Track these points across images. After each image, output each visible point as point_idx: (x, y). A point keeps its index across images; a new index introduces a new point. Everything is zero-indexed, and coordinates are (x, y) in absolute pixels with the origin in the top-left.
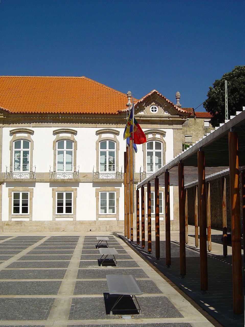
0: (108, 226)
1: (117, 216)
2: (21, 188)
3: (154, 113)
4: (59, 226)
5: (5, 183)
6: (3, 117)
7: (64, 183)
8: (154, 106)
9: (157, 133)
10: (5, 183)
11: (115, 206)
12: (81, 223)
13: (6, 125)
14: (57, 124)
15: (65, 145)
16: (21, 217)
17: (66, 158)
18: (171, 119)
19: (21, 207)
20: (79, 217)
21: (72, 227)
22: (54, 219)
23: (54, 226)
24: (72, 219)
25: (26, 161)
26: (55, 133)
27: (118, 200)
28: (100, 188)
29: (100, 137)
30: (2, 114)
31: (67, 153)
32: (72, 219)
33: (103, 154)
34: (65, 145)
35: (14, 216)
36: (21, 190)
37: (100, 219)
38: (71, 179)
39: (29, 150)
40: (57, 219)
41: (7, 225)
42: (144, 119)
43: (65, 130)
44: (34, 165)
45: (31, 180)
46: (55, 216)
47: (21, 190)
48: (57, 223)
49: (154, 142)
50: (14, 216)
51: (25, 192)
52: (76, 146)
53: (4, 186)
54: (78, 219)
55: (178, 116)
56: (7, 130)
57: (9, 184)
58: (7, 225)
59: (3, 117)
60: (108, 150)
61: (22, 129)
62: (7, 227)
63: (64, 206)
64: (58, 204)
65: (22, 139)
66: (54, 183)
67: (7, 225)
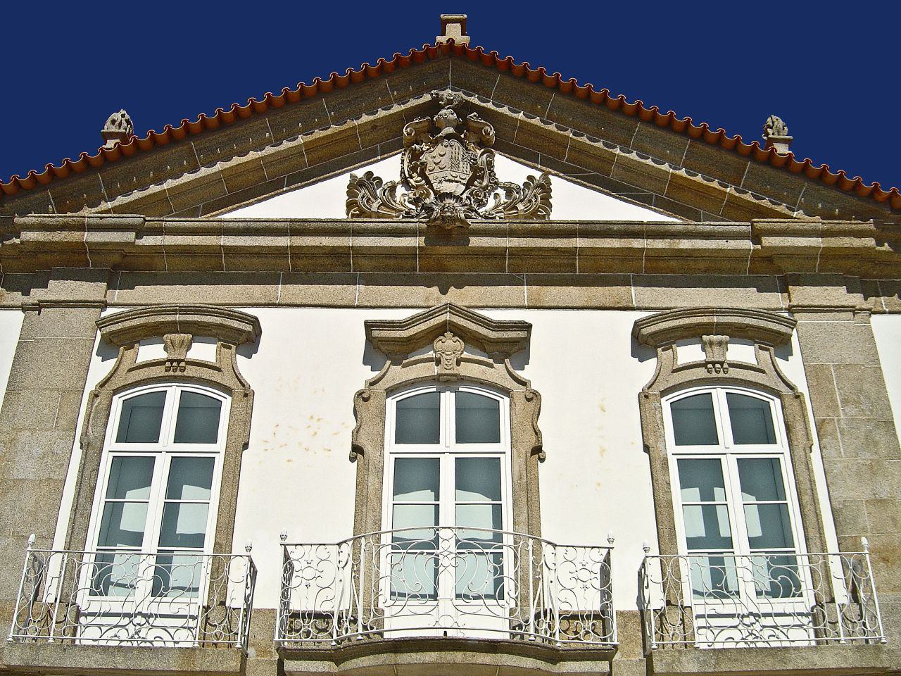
6: (870, 242)
9: (201, 332)
17: (459, 510)
30: (870, 225)
31: (467, 473)
39: (218, 449)
44: (238, 548)
49: (719, 396)
52: (243, 421)
60: (728, 450)
62: (335, 432)
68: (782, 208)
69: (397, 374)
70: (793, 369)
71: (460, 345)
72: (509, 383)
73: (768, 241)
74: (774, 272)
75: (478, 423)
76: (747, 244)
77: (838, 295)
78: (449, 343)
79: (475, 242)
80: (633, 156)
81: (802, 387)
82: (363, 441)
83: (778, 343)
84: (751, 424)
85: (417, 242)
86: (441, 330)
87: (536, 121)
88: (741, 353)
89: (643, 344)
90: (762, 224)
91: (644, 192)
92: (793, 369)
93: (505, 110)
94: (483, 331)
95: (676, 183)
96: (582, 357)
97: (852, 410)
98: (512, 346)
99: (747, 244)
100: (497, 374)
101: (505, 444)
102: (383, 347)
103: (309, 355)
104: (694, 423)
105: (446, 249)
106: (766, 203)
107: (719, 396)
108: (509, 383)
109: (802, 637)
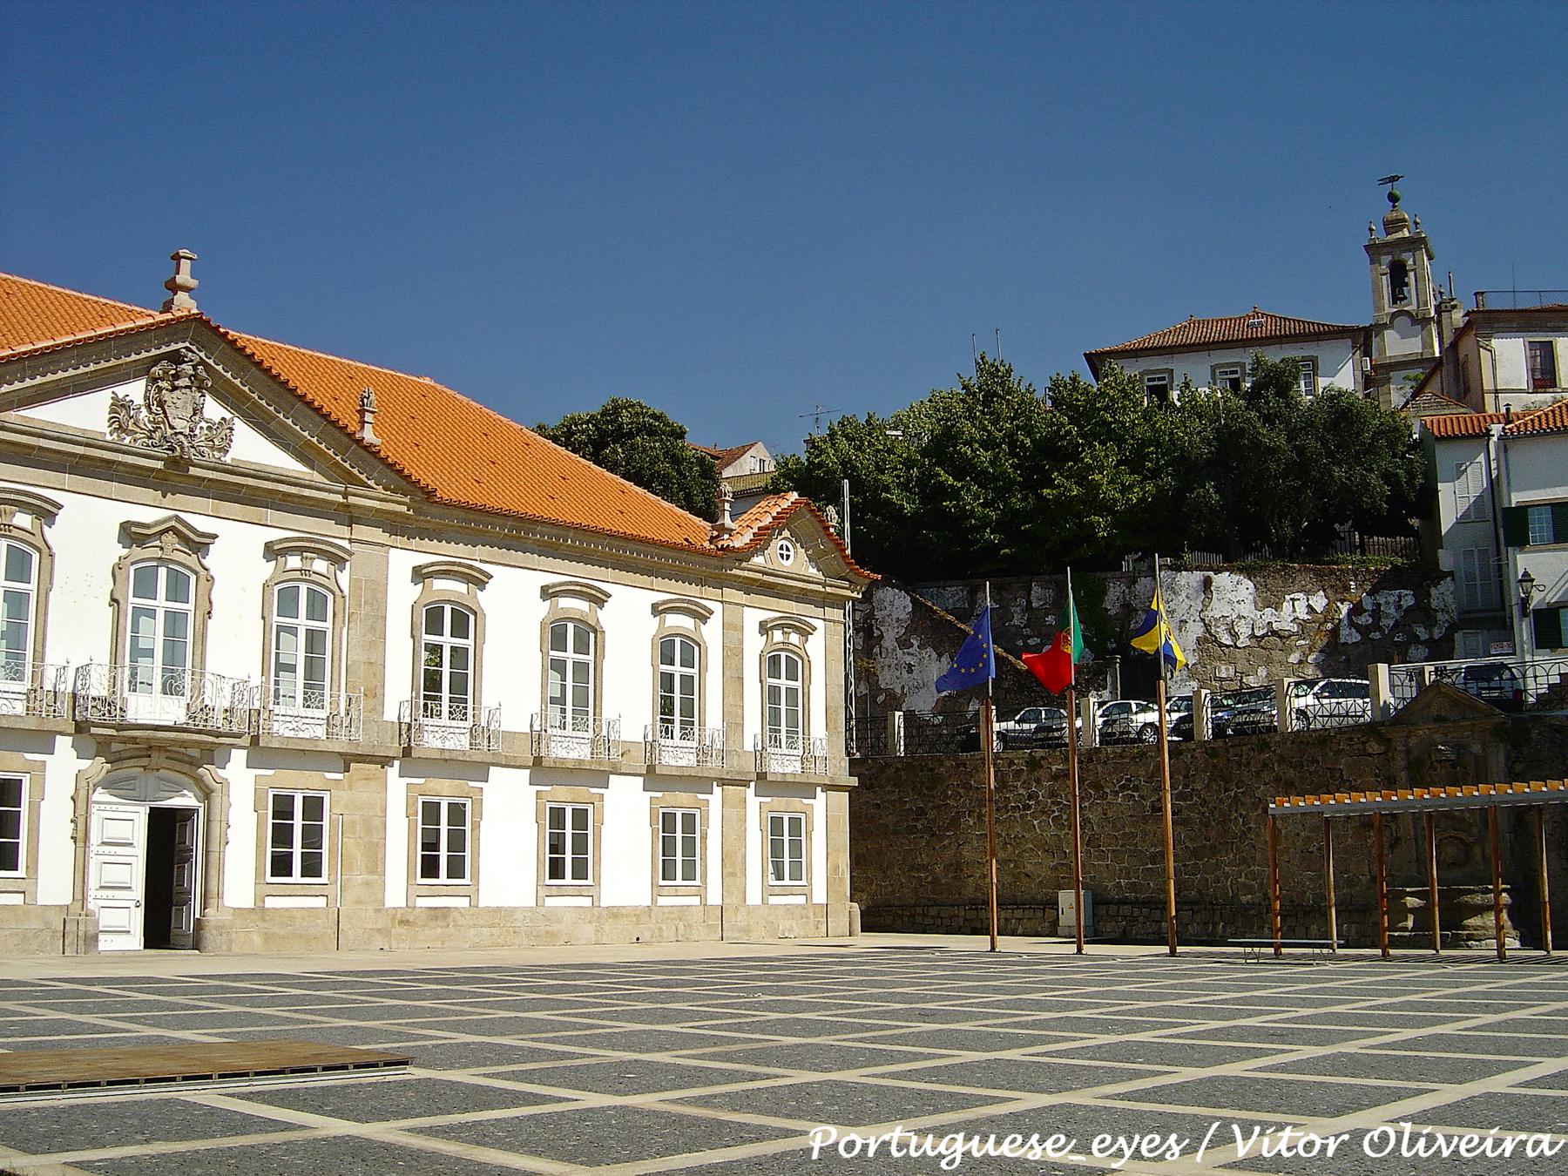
0: (681, 926)
1: (702, 893)
2: (447, 782)
3: (784, 562)
4: (556, 927)
5: (397, 763)
6: (404, 509)
7: (447, 765)
8: (785, 543)
10: (397, 763)
11: (698, 858)
12: (615, 913)
13: (399, 540)
14: (658, 582)
15: (163, 564)
16: (443, 895)
18: (829, 589)
19: (298, 822)
20: (489, 896)
21: (587, 930)
22: (260, 898)
23: (539, 923)
24: (587, 902)
25: (581, 700)
26: (547, 593)
27: (704, 837)
28: (271, 772)
29: (662, 622)
30: (407, 500)
32: (801, 900)
33: (559, 666)
34: (163, 564)
35: (425, 891)
36: (445, 791)
37: (662, 901)
38: (581, 761)
40: (550, 902)
41: (401, 922)
42: (771, 579)
43: (12, 496)
45: (32, 724)
46: (542, 892)
47: (445, 791)
48: (552, 916)
49: (303, 588)
50: (425, 891)
51: (457, 800)
53: (393, 771)
54: (485, 900)
55: (846, 584)
56: (402, 560)
57: (261, 753)
58: (404, 922)
59: (404, 509)
61: (460, 565)
62: (402, 930)
63: (567, 850)
64: (276, 842)
65: (449, 601)
66: (541, 769)
67: (401, 922)
68: (371, 482)
69: (138, 553)
70: (344, 578)
71: (176, 540)
72: (198, 568)
73: (352, 500)
74: (349, 516)
75: (177, 589)
76: (339, 498)
77: (377, 534)
78: (170, 538)
79: (193, 471)
80: (289, 421)
81: (346, 593)
82: (116, 596)
83: (337, 560)
84: (317, 608)
85: (159, 465)
86: (172, 529)
87: (237, 382)
88: (320, 565)
89: (272, 552)
90: (351, 489)
91: (760, 1134)
92: (344, 578)
93: (220, 368)
94: (192, 536)
95: (309, 444)
96: (239, 550)
97: (368, 608)
98: (199, 544)
99: (339, 498)
100: (192, 560)
101: (190, 606)
102: (131, 534)
103: (88, 529)
104: (288, 602)
105: (174, 473)
106: (363, 477)
107: (303, 588)
108: (198, 568)
109: (321, 732)
